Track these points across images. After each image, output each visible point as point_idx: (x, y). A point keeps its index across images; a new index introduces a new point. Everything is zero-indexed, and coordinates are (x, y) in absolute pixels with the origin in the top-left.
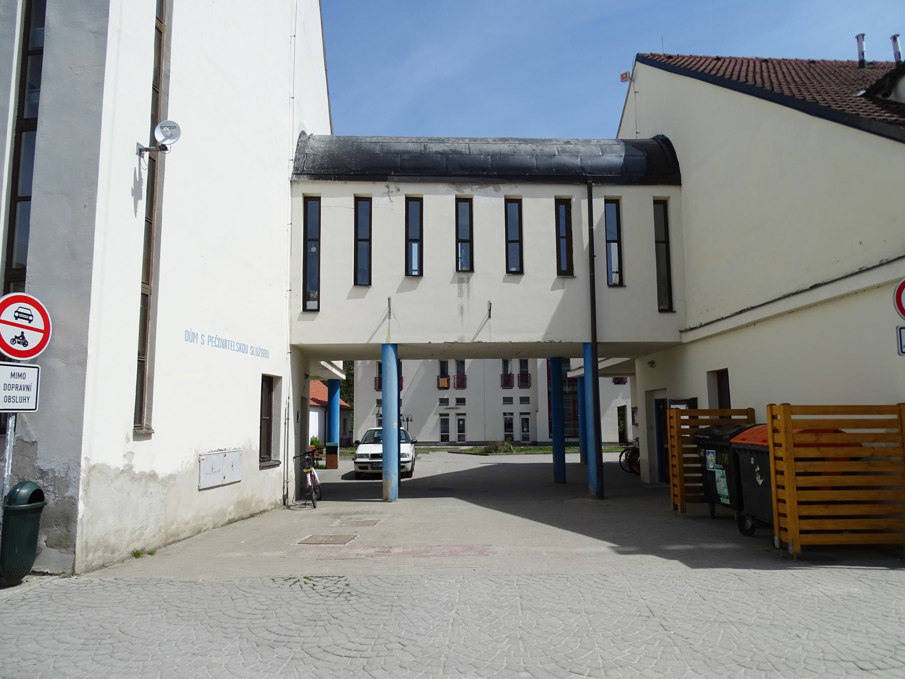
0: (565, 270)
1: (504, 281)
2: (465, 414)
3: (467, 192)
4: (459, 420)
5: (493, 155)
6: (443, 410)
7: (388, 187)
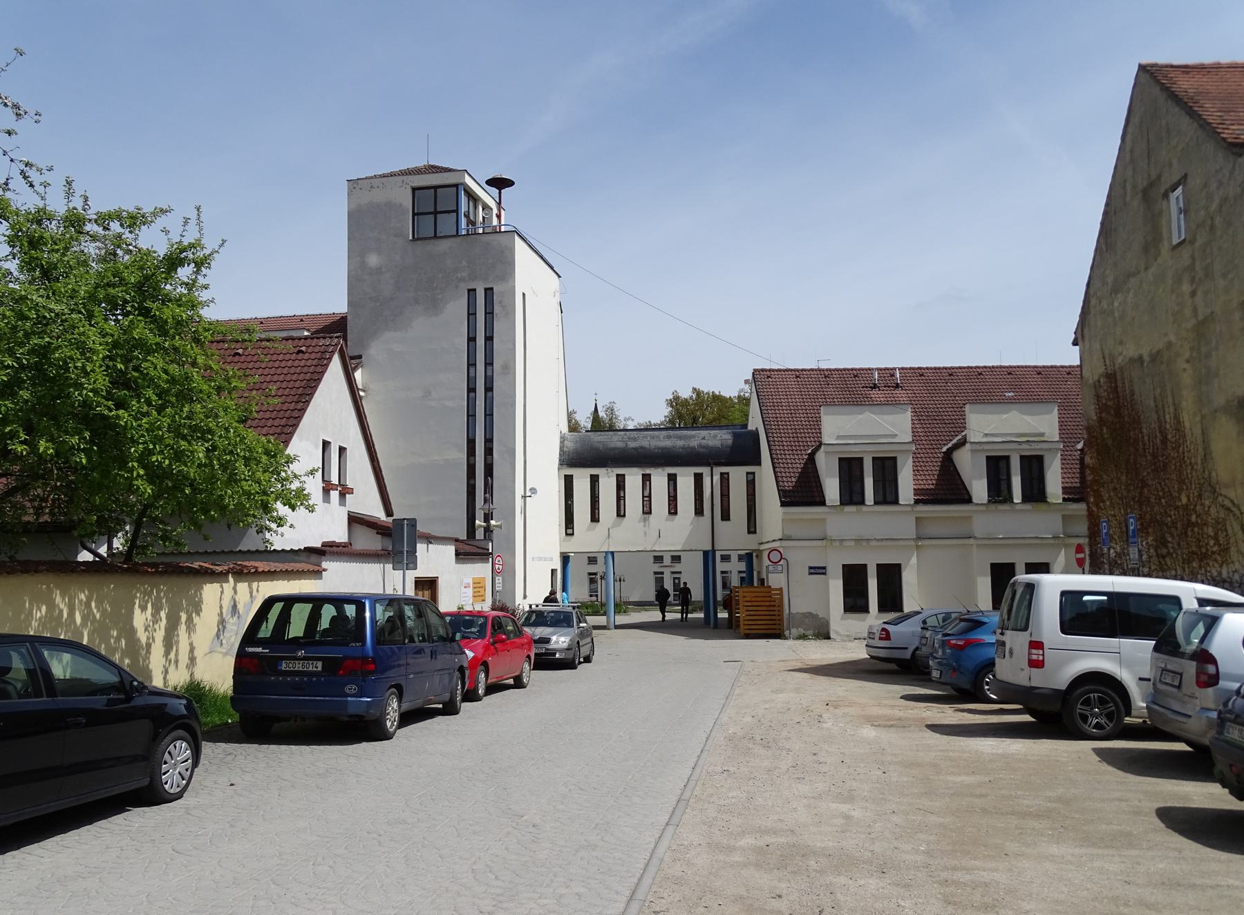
0: (699, 511)
1: (667, 520)
2: (680, 573)
3: (648, 471)
4: (675, 578)
5: (662, 448)
6: (656, 568)
7: (607, 470)
